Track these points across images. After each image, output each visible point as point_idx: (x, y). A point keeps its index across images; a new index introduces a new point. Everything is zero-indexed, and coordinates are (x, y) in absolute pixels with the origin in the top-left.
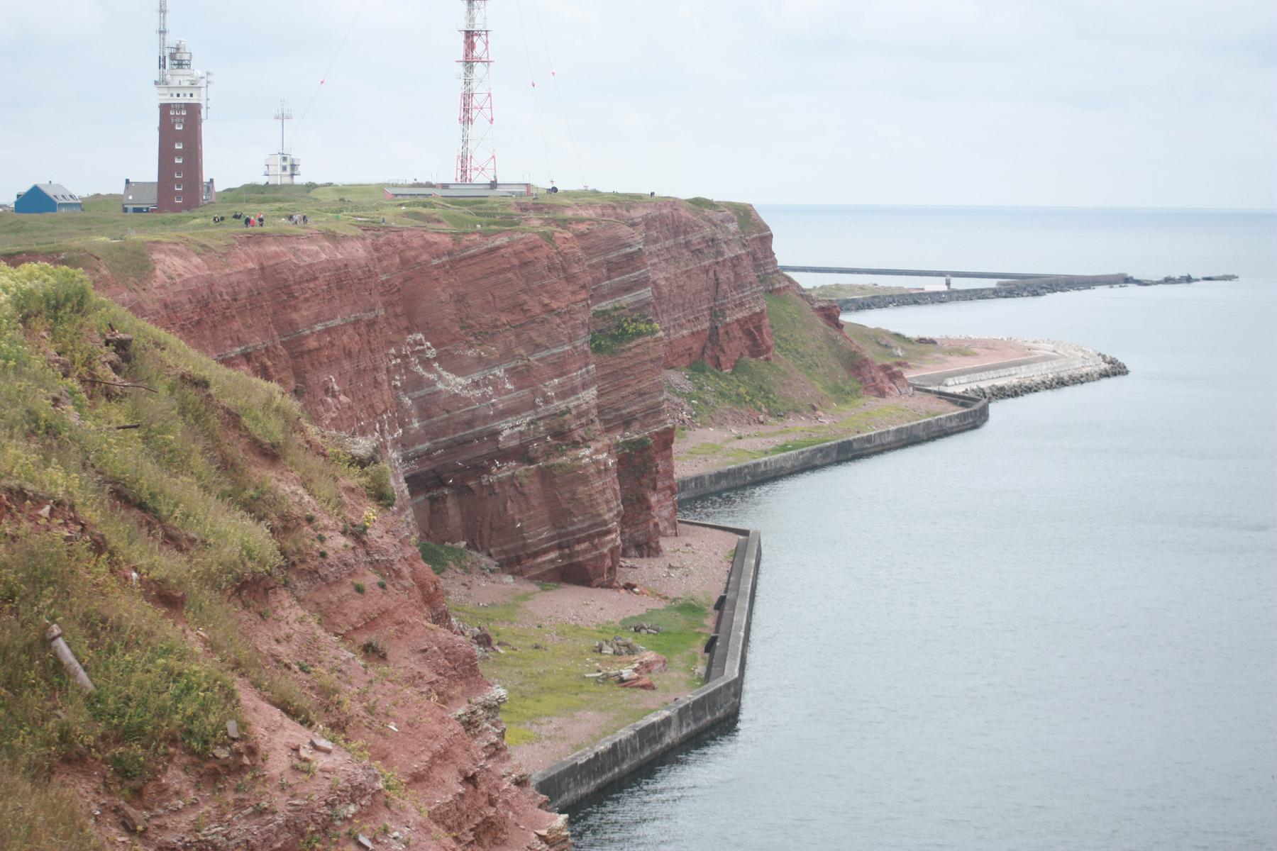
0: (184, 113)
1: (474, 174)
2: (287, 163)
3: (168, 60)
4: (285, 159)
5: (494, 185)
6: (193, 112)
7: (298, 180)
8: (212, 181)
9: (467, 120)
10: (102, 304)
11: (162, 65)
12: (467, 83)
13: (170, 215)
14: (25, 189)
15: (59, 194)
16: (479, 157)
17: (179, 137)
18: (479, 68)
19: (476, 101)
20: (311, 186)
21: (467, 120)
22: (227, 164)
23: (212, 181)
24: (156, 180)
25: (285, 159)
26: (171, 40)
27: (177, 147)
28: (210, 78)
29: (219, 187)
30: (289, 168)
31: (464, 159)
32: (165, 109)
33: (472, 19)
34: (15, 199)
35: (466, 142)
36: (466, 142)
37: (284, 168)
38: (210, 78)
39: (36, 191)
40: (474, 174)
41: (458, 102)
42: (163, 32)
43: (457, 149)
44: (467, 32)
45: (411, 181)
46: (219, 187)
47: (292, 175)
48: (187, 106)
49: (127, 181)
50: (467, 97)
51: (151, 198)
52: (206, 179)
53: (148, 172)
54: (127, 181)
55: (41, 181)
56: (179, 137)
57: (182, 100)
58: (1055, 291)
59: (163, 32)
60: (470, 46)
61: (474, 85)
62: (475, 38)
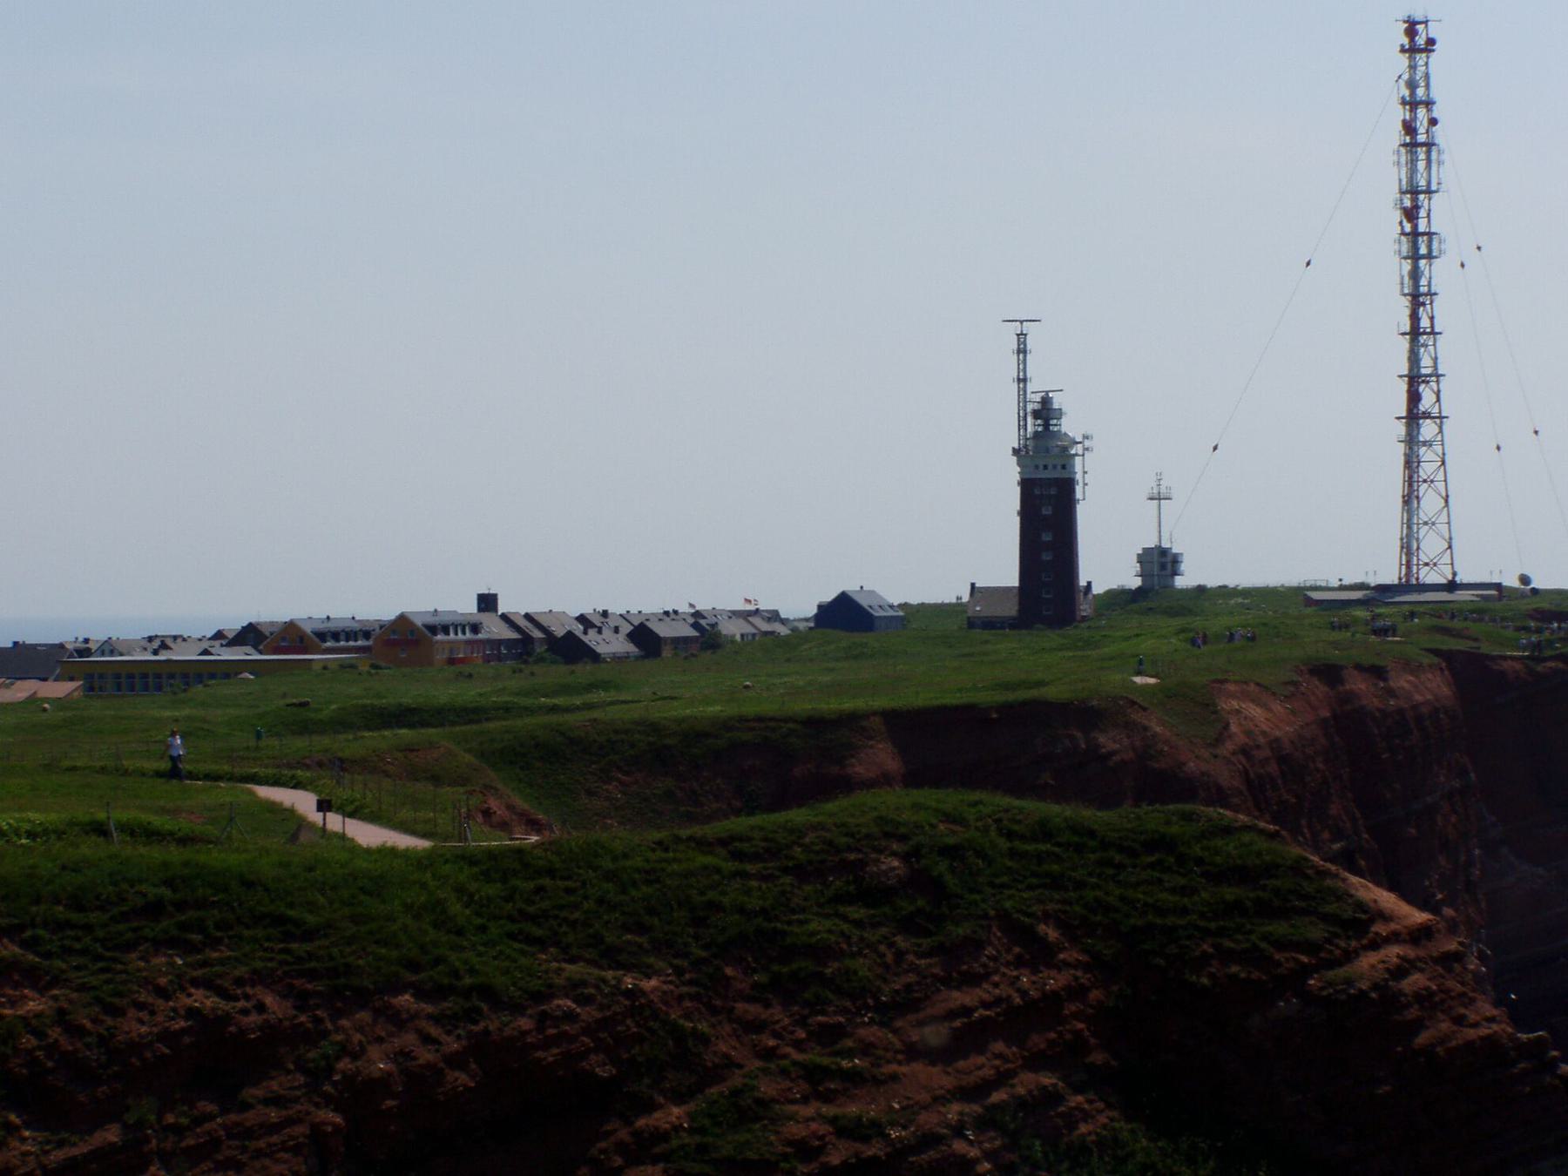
0: (1053, 492)
5: (1452, 586)
8: (1089, 583)
10: (729, 1064)
13: (1423, 213)
14: (829, 596)
15: (874, 603)
18: (1427, 429)
19: (1427, 469)
20: (1201, 590)
22: (1105, 563)
23: (1089, 583)
26: (1036, 386)
28: (1087, 443)
29: (1097, 589)
32: (1027, 485)
34: (815, 611)
38: (1087, 443)
39: (844, 600)
42: (1022, 380)
45: (1336, 584)
46: (1097, 589)
49: (973, 585)
51: (1011, 609)
52: (1083, 583)
53: (1006, 573)
54: (973, 585)
55: (850, 587)
59: (1022, 380)
60: (1414, 398)
62: (1422, 387)
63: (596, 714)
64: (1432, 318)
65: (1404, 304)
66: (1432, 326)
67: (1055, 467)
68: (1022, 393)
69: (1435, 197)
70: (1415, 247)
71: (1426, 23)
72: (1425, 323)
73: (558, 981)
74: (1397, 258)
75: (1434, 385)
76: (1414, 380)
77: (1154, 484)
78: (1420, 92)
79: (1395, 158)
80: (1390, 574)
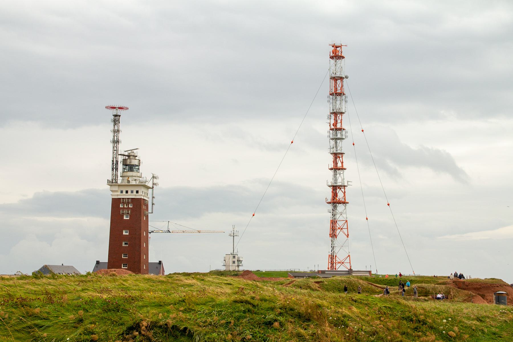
1: (338, 266)
2: (236, 260)
3: (120, 166)
4: (234, 257)
5: (350, 272)
6: (139, 207)
7: (241, 269)
9: (333, 235)
11: (115, 168)
12: (334, 215)
16: (340, 256)
17: (126, 225)
19: (339, 224)
21: (333, 235)
22: (178, 248)
24: (107, 261)
25: (234, 257)
26: (123, 148)
27: (124, 233)
28: (155, 181)
30: (236, 262)
31: (332, 257)
32: (116, 202)
33: (336, 180)
35: (333, 248)
36: (333, 248)
37: (234, 262)
38: (155, 181)
40: (338, 266)
41: (328, 225)
42: (116, 142)
43: (328, 251)
44: (333, 186)
47: (238, 266)
48: (134, 200)
50: (334, 222)
56: (126, 225)
57: (130, 196)
58: (41, 269)
59: (116, 142)
60: (335, 195)
61: (337, 216)
62: (338, 190)
63: (424, 285)
64: (342, 163)
65: (331, 158)
66: (342, 166)
67: (132, 192)
68: (115, 150)
69: (343, 115)
70: (335, 195)
71: (340, 47)
72: (339, 165)
73: (222, 330)
74: (329, 139)
75: (343, 190)
76: (335, 188)
77: (232, 229)
78: (339, 126)
79: (328, 134)
80: (325, 266)
